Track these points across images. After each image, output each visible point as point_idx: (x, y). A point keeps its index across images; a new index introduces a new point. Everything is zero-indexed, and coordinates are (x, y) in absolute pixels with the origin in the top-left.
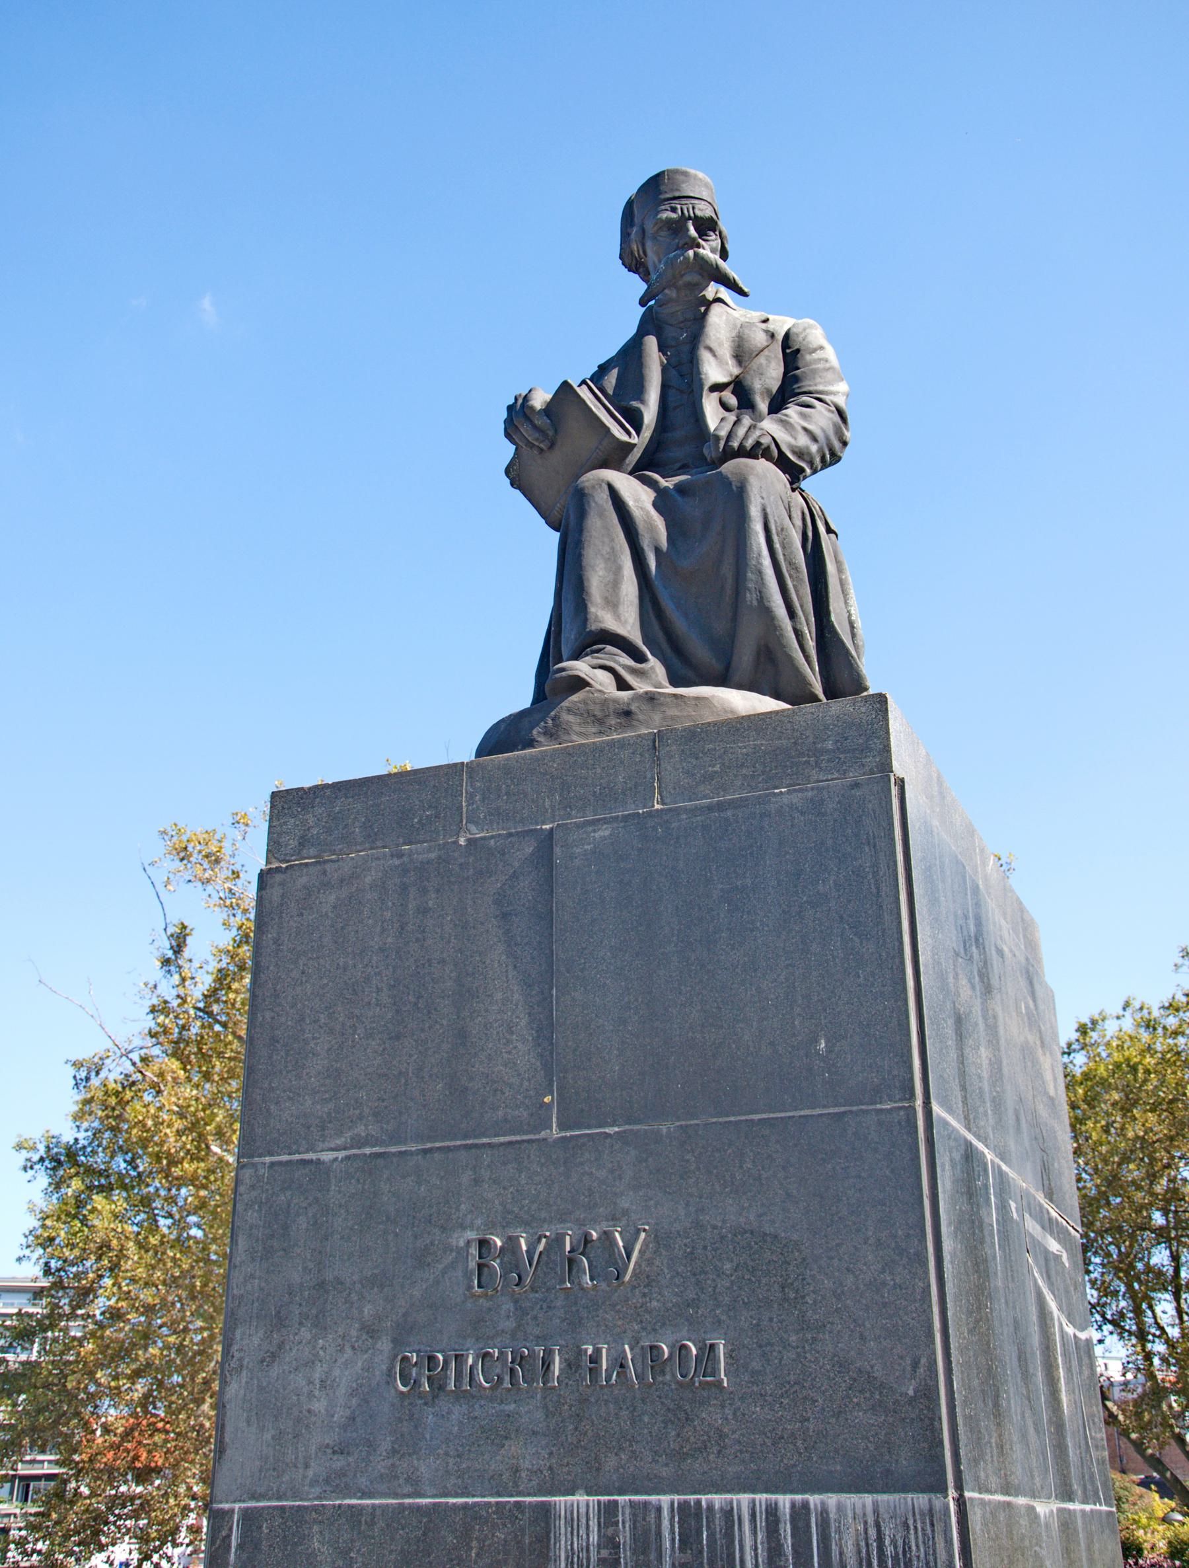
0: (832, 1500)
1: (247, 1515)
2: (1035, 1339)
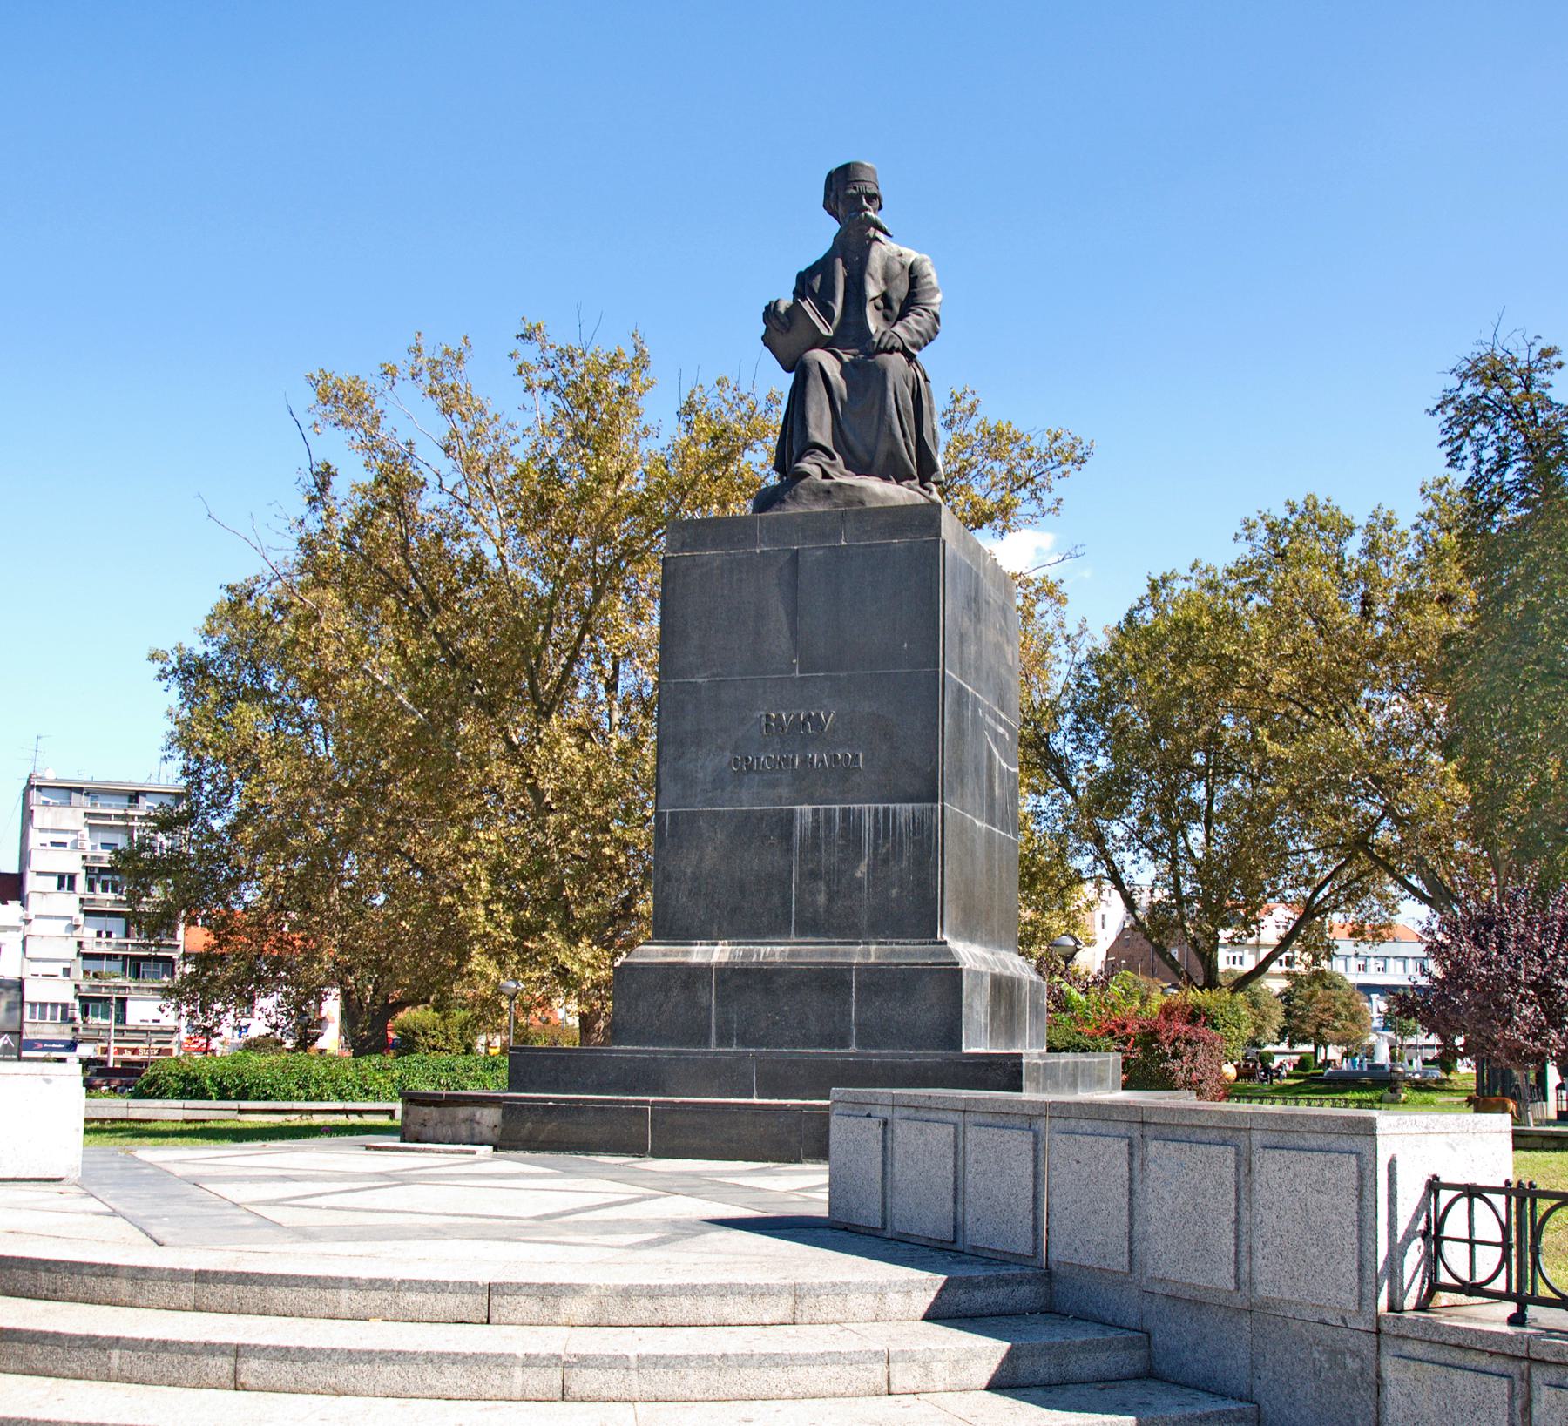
0: (898, 806)
2: (985, 763)
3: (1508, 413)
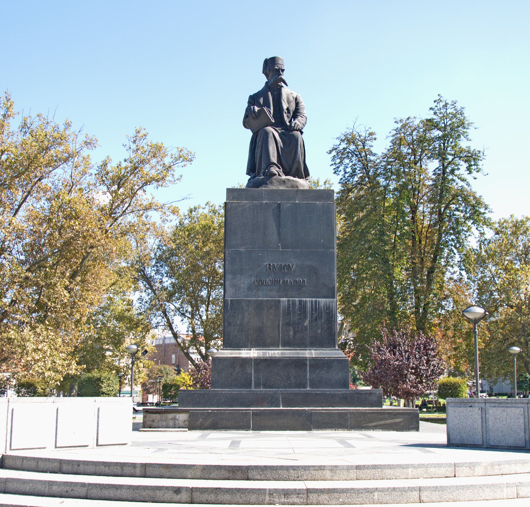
0: (320, 299)
1: (231, 300)
3: (356, 155)
